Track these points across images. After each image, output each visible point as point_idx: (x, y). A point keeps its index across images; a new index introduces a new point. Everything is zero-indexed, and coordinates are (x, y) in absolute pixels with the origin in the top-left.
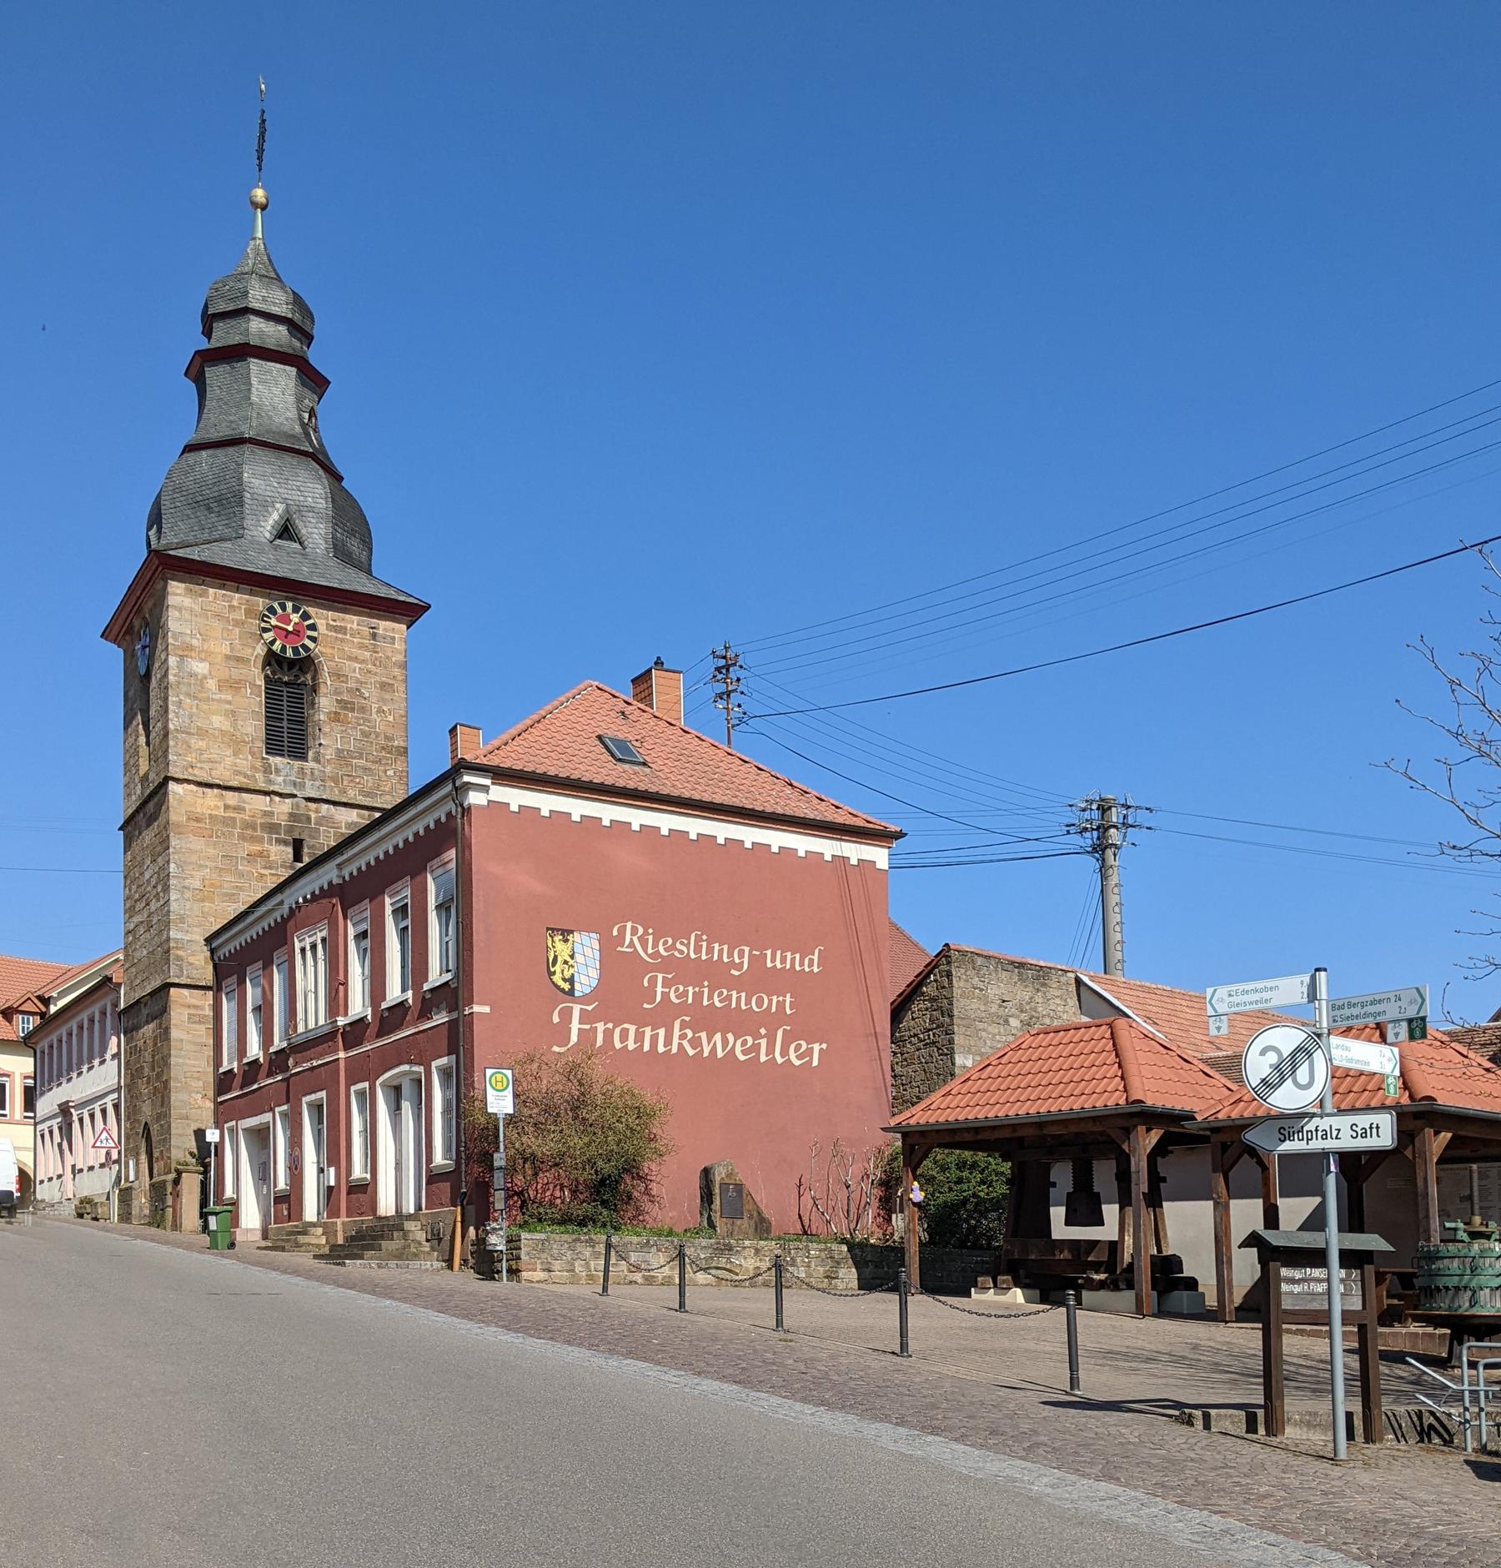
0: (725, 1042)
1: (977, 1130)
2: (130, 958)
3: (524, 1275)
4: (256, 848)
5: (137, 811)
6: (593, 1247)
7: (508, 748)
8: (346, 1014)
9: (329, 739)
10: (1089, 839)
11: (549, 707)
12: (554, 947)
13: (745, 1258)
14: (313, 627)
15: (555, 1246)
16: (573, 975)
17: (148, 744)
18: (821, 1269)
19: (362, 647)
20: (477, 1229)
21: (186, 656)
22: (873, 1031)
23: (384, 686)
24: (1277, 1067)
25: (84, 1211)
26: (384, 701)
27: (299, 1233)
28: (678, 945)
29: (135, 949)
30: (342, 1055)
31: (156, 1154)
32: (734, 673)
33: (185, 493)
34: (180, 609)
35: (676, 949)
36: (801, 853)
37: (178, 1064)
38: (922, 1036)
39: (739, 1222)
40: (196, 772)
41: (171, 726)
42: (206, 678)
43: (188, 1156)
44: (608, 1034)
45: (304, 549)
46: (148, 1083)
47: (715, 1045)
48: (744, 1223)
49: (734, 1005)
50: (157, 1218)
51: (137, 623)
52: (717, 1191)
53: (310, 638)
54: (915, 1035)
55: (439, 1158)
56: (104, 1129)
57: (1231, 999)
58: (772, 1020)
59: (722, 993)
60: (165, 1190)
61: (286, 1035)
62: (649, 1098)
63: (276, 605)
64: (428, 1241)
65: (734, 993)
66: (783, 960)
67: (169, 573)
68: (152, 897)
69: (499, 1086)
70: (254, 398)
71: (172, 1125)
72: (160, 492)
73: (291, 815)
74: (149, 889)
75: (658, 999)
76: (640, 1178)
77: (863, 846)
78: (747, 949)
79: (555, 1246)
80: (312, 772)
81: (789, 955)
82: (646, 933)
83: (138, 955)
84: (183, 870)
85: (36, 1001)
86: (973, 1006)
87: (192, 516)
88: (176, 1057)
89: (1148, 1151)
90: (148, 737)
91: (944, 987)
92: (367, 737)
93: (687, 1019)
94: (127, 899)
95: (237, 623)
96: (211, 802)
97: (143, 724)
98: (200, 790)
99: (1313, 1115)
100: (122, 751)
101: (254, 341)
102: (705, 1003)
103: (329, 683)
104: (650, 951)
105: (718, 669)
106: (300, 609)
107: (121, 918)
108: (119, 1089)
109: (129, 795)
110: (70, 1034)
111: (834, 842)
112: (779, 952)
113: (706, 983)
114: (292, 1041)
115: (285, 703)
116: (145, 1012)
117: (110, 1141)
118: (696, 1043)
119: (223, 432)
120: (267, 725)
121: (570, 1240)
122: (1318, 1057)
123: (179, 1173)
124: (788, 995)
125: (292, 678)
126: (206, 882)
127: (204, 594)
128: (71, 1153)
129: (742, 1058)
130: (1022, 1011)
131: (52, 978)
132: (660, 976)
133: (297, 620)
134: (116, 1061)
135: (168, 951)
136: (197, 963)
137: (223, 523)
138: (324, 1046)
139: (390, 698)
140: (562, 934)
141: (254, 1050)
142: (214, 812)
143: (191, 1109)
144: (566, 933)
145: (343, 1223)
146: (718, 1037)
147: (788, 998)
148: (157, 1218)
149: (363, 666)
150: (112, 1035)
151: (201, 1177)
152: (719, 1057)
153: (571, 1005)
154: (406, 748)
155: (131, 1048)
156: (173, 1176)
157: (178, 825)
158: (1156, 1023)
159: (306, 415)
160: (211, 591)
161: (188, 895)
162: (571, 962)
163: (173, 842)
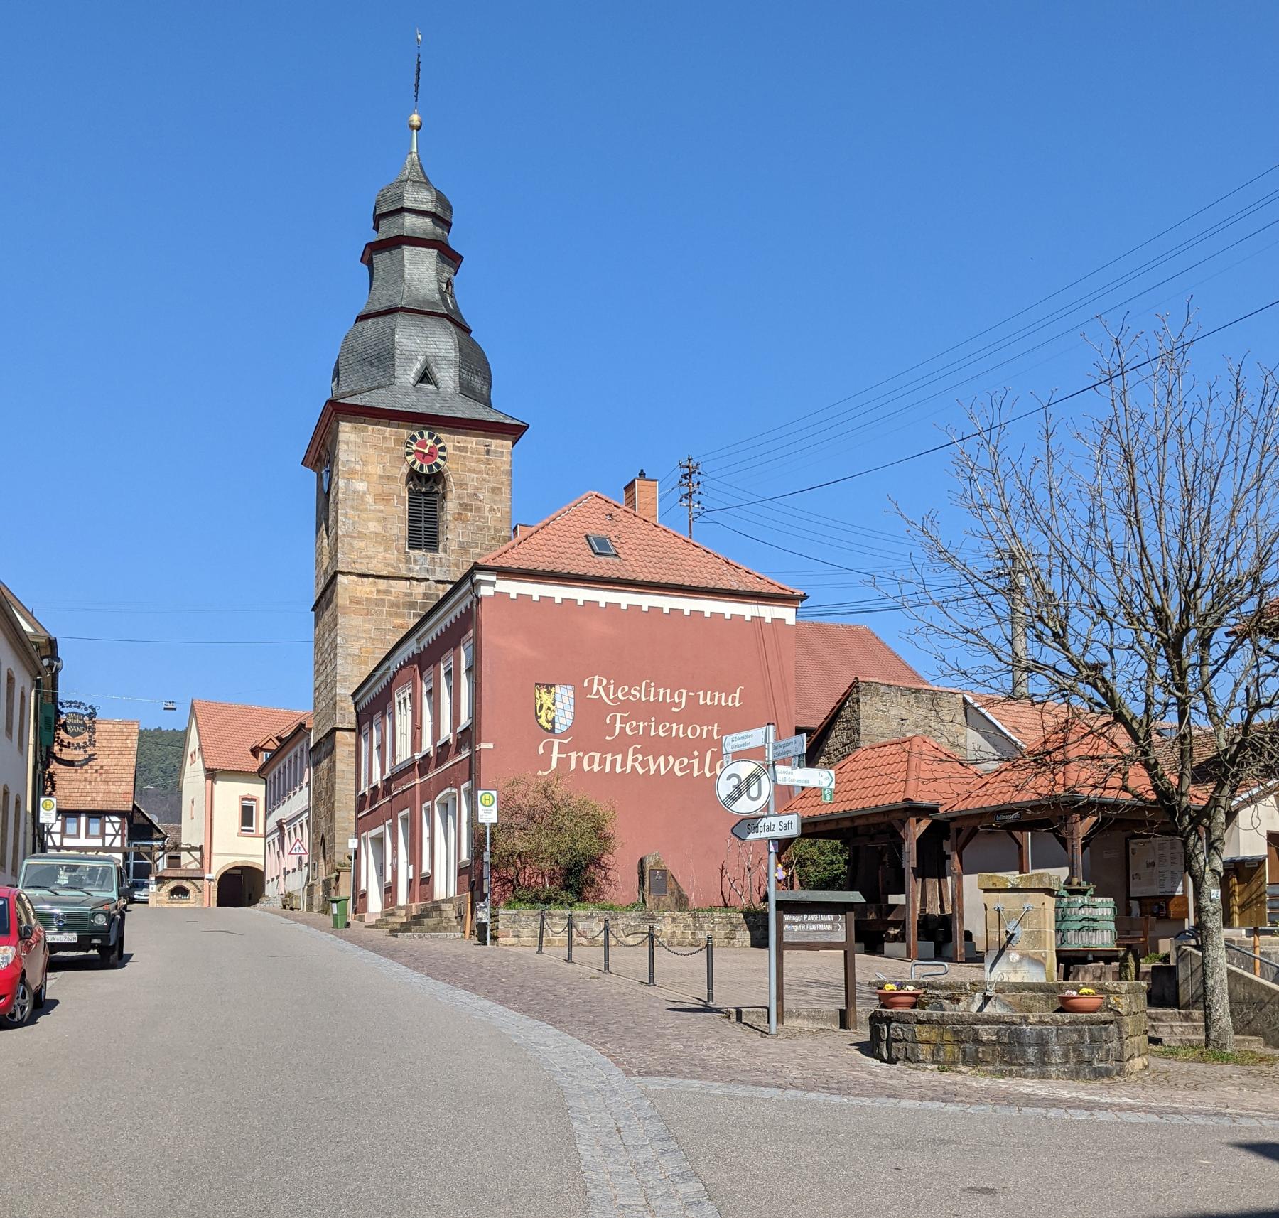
0: (667, 763)
1: (815, 824)
3: (500, 940)
5: (321, 597)
7: (514, 551)
8: (421, 751)
9: (453, 534)
11: (553, 516)
13: (665, 925)
14: (443, 449)
15: (523, 919)
16: (554, 718)
18: (723, 932)
19: (479, 461)
21: (352, 478)
23: (495, 490)
24: (737, 787)
26: (495, 502)
28: (633, 692)
30: (418, 781)
32: (695, 478)
34: (347, 443)
35: (631, 694)
36: (728, 616)
37: (340, 789)
38: (841, 750)
39: (663, 898)
42: (365, 494)
43: (347, 859)
44: (579, 760)
47: (659, 765)
48: (668, 899)
49: (674, 735)
51: (323, 453)
52: (647, 875)
53: (441, 457)
54: (837, 749)
55: (464, 857)
57: (734, 743)
59: (665, 726)
62: (603, 808)
63: (417, 434)
66: (712, 699)
69: (488, 803)
70: (406, 276)
73: (425, 594)
76: (601, 867)
77: (775, 608)
78: (684, 692)
79: (523, 919)
81: (717, 694)
82: (609, 683)
85: (276, 741)
86: (876, 725)
88: (339, 784)
89: (918, 836)
91: (854, 711)
93: (639, 746)
94: (316, 663)
95: (389, 450)
96: (367, 588)
99: (763, 817)
101: (407, 232)
102: (652, 734)
103: (454, 491)
104: (611, 697)
105: (684, 476)
107: (313, 678)
108: (308, 810)
109: (318, 584)
111: (752, 606)
112: (709, 693)
113: (653, 719)
115: (423, 509)
116: (323, 750)
117: (302, 849)
118: (644, 764)
120: (410, 526)
121: (534, 914)
122: (764, 779)
124: (716, 725)
126: (363, 649)
127: (365, 430)
129: (679, 774)
130: (917, 727)
131: (290, 722)
132: (619, 716)
133: (431, 444)
135: (335, 704)
140: (547, 688)
142: (369, 596)
145: (416, 907)
146: (661, 759)
147: (716, 727)
157: (344, 607)
158: (1020, 732)
159: (444, 285)
161: (350, 660)
162: (553, 708)
163: (340, 621)
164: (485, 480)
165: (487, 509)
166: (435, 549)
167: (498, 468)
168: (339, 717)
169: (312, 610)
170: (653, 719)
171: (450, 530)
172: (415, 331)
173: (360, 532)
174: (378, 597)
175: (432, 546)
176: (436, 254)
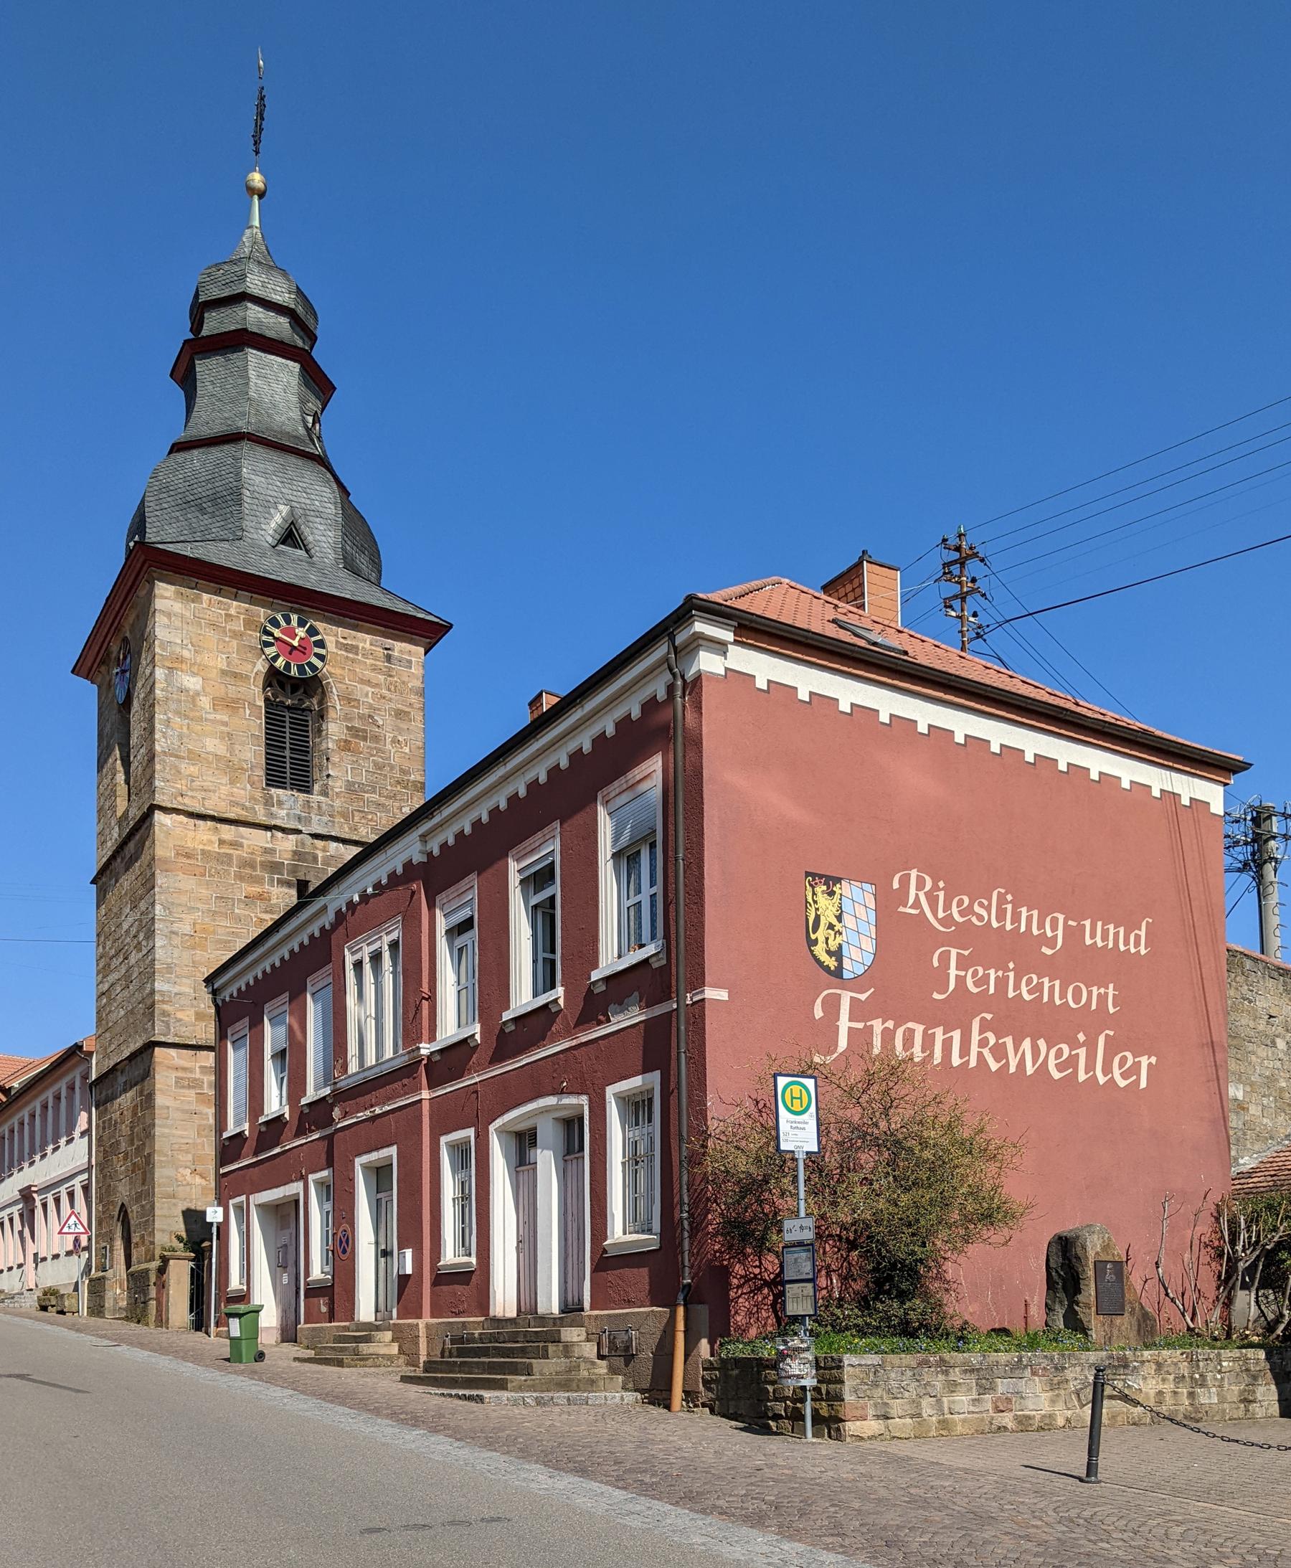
0: (1036, 1052)
2: (104, 1022)
3: (851, 1427)
4: (256, 889)
5: (113, 857)
6: (946, 1373)
8: (432, 1038)
10: (1243, 853)
12: (815, 902)
13: (1145, 1378)
16: (840, 946)
17: (127, 782)
18: (1235, 1388)
19: (375, 669)
20: (712, 1343)
21: (176, 669)
22: (1209, 1041)
23: (399, 714)
25: (47, 1303)
26: (400, 730)
27: (358, 1340)
28: (977, 908)
29: (110, 1012)
30: (425, 1094)
31: (135, 1238)
32: (973, 567)
33: (172, 493)
34: (169, 615)
35: (975, 914)
37: (163, 1135)
39: (1118, 1320)
40: (186, 801)
41: (158, 748)
42: (198, 694)
43: (175, 1240)
44: (888, 1036)
45: (311, 557)
46: (125, 1158)
48: (1125, 1323)
49: (1046, 999)
50: (136, 1312)
51: (115, 648)
53: (317, 655)
56: (73, 1213)
58: (1093, 1020)
60: (148, 1279)
61: (328, 1078)
63: (279, 617)
64: (601, 1357)
65: (1046, 980)
66: (1105, 937)
67: (157, 572)
68: (132, 948)
71: (157, 1204)
72: (144, 497)
73: (295, 853)
74: (128, 940)
75: (952, 986)
77: (1196, 781)
78: (1061, 917)
79: (893, 1375)
80: (319, 807)
82: (935, 887)
83: (113, 1017)
84: (170, 912)
87: (181, 518)
88: (160, 1126)
90: (127, 773)
92: (380, 769)
93: (989, 1016)
95: (236, 635)
96: (203, 836)
97: (122, 760)
98: (192, 821)
100: (96, 796)
102: (1011, 994)
104: (941, 915)
106: (307, 622)
110: (33, 1116)
114: (338, 1086)
115: (287, 730)
117: (79, 1226)
118: (999, 1052)
119: (217, 429)
120: (267, 753)
121: (914, 1364)
123: (165, 1260)
124: (1111, 986)
125: (296, 702)
127: (196, 600)
128: (34, 1241)
129: (1056, 1075)
131: (13, 1071)
132: (954, 952)
134: (87, 1138)
135: (153, 1005)
136: (186, 1019)
137: (218, 524)
138: (395, 1085)
139: (406, 727)
141: (275, 1102)
143: (179, 1185)
144: (831, 881)
145: (428, 1326)
146: (1027, 1044)
148: (136, 1312)
149: (377, 690)
150: (81, 1110)
151: (191, 1264)
152: (1028, 1073)
153: (838, 991)
154: (423, 784)
155: (104, 1122)
156: (155, 1264)
157: (165, 861)
159: (310, 419)
160: (205, 596)
161: (176, 941)
162: (838, 927)
164: (384, 698)
165: (389, 740)
166: (307, 789)
167: (404, 683)
168: (159, 1027)
169: (92, 883)
170: (1011, 965)
171: (334, 764)
172: (273, 469)
173: (190, 751)
174: (222, 851)
175: (303, 784)
176: (297, 370)
